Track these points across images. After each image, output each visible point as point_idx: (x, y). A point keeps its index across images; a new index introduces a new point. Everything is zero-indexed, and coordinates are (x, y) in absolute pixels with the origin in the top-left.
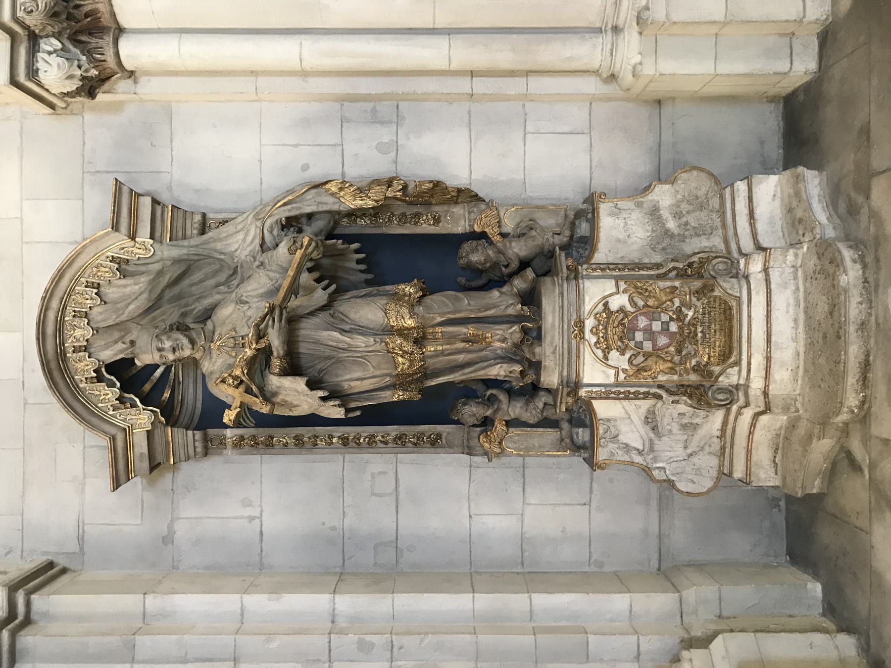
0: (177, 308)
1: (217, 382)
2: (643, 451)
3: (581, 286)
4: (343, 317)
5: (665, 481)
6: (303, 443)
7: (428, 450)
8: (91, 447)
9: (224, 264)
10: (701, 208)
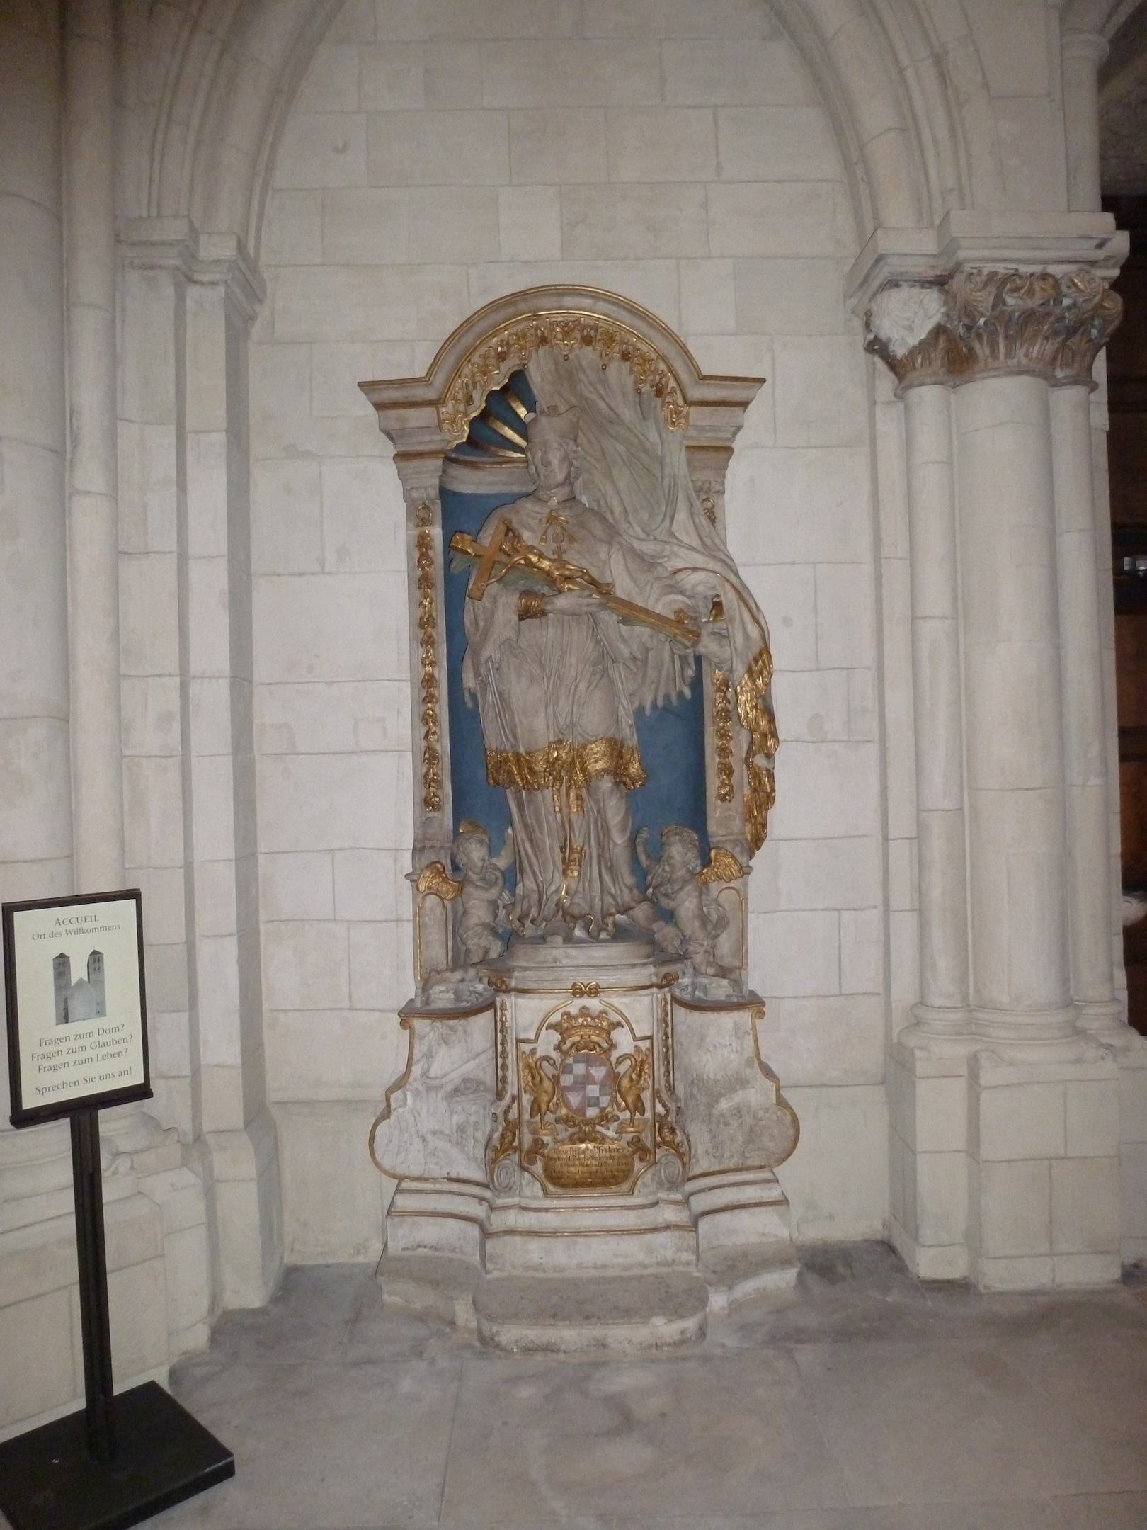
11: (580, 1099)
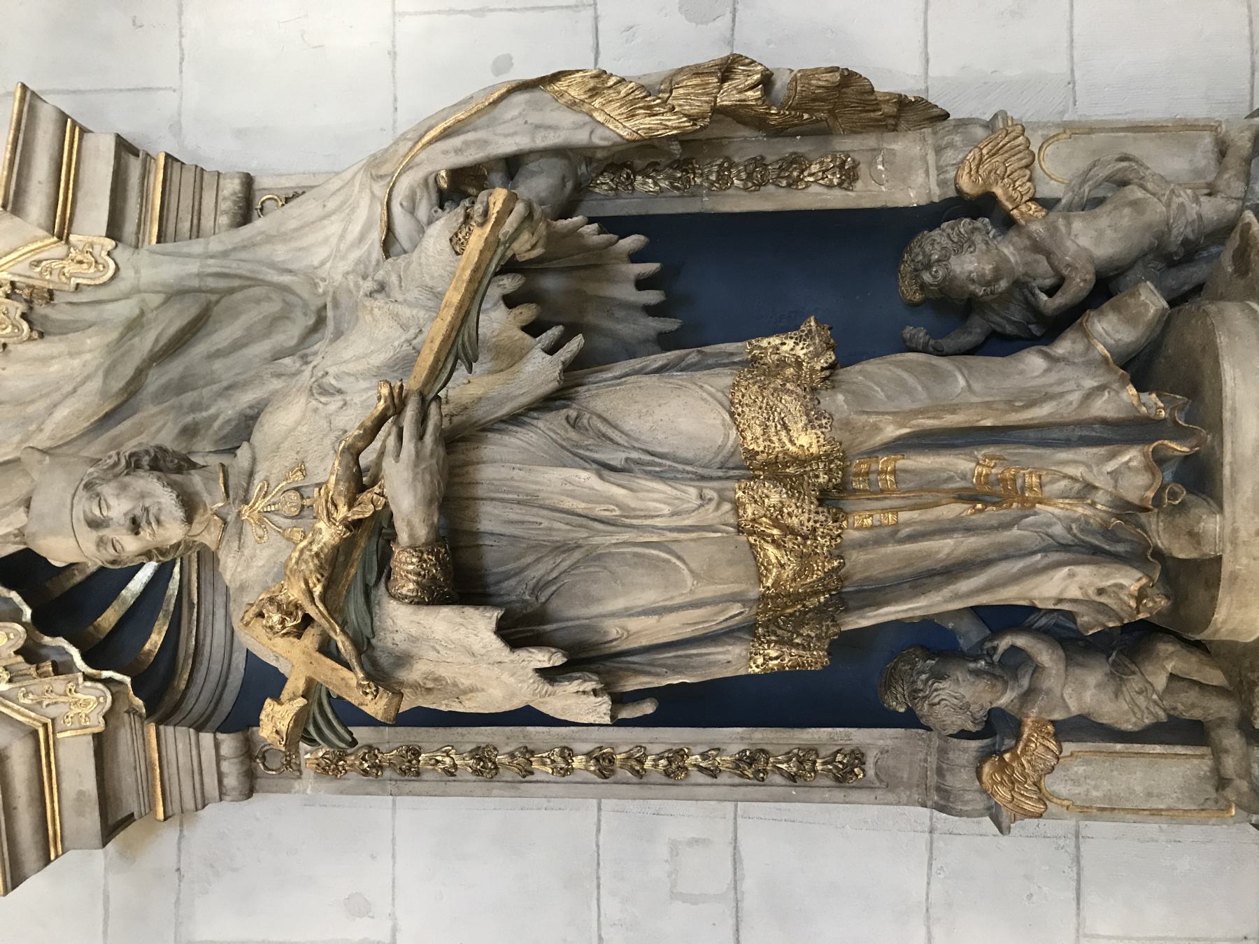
0: (171, 416)
1: (247, 618)
4: (604, 428)
6: (496, 768)
9: (291, 298)
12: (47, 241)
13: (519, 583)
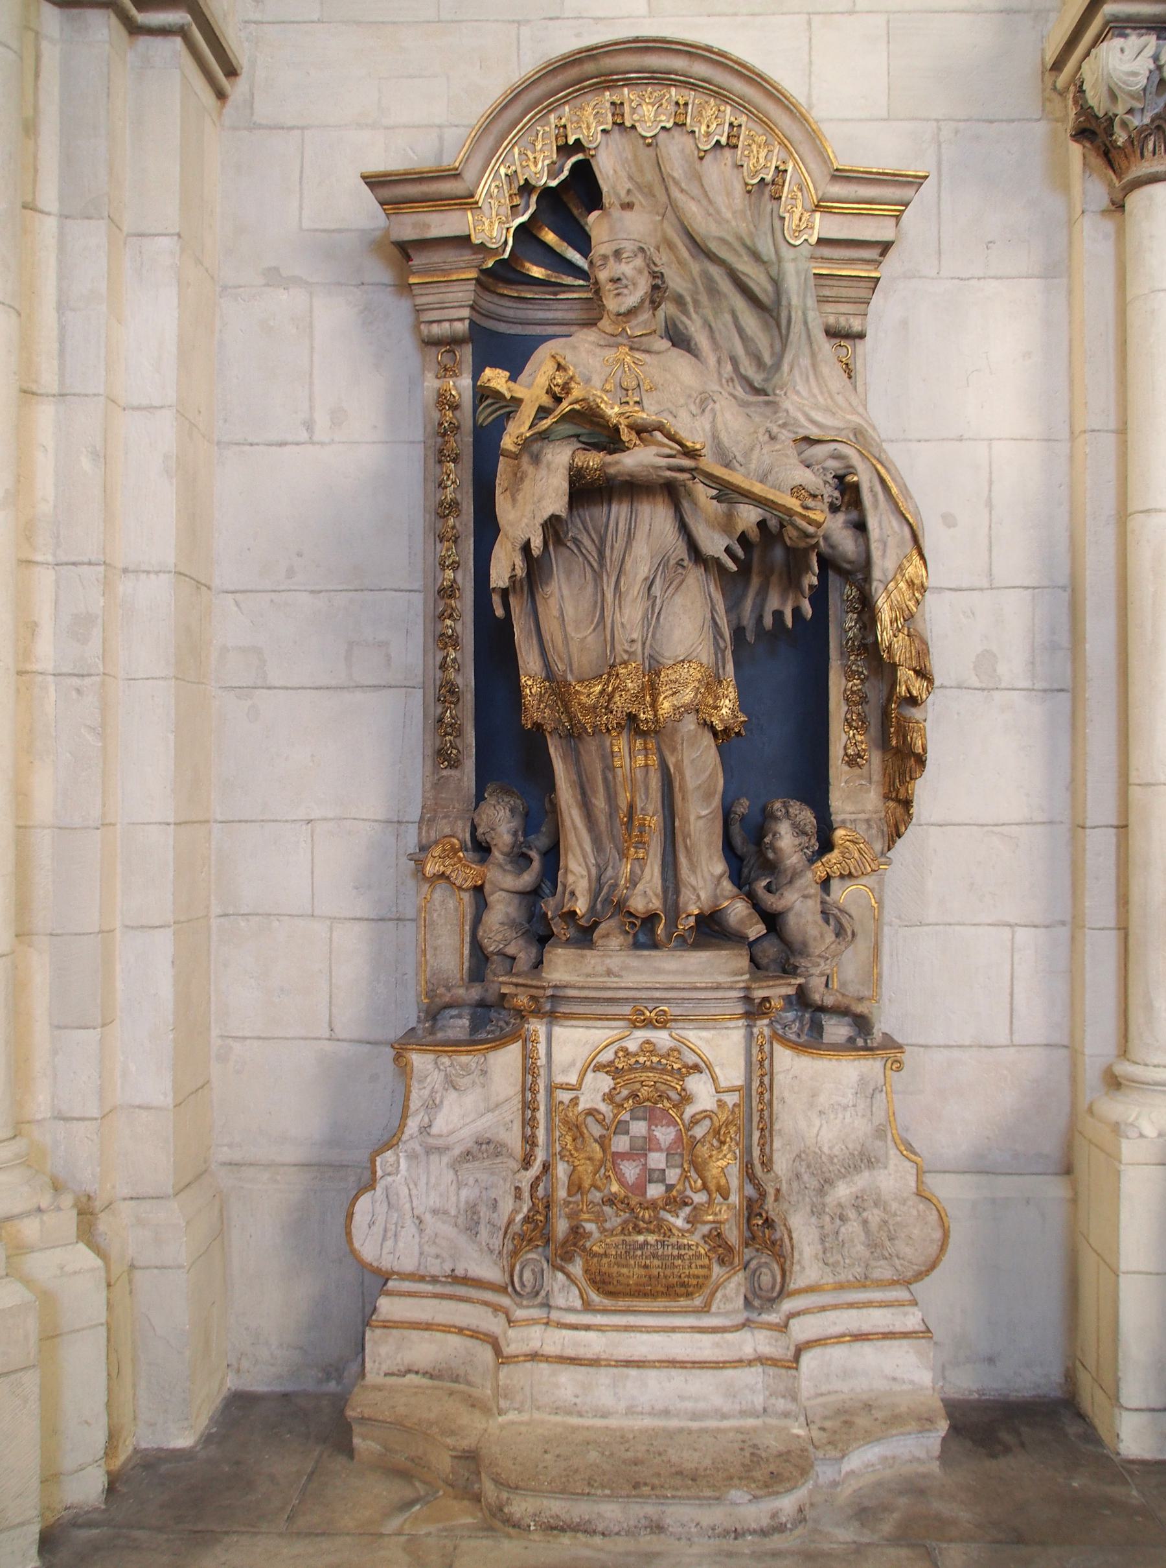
1: (558, 357)
2: (429, 1134)
3: (732, 1024)
5: (374, 1173)
6: (445, 517)
7: (429, 743)
8: (441, 138)
10: (873, 1246)
11: (638, 1171)
12: (814, 197)
13: (579, 529)
